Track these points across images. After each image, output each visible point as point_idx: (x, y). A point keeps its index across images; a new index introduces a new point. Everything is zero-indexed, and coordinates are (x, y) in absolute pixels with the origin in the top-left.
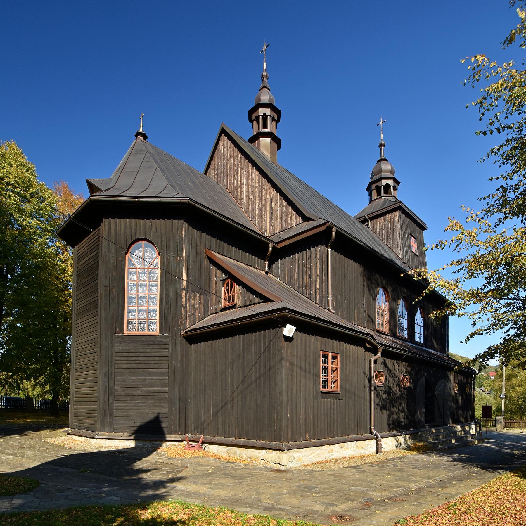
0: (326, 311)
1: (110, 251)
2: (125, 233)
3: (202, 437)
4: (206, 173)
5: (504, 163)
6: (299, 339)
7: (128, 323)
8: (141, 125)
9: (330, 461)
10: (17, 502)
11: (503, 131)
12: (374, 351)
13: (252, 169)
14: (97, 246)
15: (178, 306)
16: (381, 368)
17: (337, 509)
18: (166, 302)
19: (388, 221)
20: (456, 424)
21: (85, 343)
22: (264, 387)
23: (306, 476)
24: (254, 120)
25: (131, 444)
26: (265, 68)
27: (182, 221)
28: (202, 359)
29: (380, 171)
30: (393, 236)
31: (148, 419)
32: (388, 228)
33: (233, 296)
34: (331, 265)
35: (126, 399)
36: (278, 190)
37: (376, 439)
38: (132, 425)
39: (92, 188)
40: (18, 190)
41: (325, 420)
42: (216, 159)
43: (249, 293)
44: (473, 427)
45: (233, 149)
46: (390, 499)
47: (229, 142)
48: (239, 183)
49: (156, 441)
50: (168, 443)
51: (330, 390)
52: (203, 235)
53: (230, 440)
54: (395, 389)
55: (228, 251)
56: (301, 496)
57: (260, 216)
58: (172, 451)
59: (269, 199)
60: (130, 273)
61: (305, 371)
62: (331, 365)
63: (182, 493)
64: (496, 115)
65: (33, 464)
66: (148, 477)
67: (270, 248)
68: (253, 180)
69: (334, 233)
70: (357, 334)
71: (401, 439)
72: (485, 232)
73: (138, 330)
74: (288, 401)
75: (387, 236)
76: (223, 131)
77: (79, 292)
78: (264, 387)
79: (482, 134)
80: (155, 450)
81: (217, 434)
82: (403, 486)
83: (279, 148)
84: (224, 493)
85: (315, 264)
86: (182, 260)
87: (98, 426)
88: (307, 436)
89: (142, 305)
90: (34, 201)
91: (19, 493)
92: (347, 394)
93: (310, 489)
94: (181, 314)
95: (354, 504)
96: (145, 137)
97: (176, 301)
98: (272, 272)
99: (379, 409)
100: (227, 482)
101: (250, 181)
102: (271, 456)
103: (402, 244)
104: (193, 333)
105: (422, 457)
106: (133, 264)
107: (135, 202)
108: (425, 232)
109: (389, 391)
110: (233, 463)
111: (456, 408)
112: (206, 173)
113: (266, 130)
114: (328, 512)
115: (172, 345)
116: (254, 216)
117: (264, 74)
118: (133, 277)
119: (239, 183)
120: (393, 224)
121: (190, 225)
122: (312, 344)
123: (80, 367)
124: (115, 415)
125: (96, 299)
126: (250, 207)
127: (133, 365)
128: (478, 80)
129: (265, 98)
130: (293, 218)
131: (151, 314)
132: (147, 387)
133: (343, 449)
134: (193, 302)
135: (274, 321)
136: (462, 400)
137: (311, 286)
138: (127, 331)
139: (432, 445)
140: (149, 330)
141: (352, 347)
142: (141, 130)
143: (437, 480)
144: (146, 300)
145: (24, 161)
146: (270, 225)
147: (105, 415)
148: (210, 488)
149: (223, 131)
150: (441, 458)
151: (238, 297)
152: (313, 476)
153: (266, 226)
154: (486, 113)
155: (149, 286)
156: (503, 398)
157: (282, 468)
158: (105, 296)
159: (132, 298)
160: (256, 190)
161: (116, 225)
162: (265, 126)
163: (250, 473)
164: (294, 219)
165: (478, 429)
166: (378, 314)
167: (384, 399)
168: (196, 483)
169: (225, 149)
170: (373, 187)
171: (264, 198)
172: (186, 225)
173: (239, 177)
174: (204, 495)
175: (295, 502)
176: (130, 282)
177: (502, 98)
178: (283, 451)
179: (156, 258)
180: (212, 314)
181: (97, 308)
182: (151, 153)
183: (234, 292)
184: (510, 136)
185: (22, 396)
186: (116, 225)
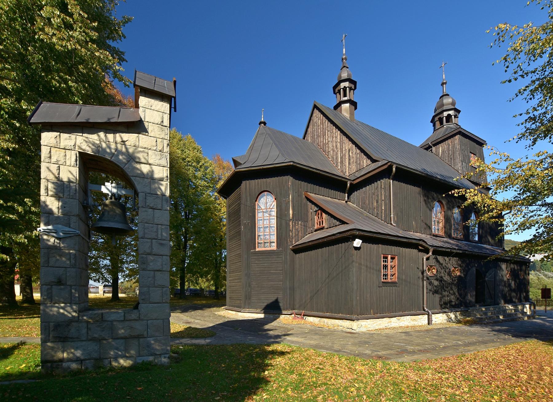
0: (389, 225)
1: (247, 201)
2: (255, 189)
3: (303, 312)
4: (304, 138)
5: (531, 99)
7: (258, 243)
10: (208, 341)
12: (426, 251)
14: (239, 198)
15: (288, 230)
16: (432, 262)
17: (379, 353)
18: (280, 229)
19: (449, 145)
20: (508, 303)
22: (342, 279)
23: (367, 336)
25: (262, 316)
29: (443, 105)
30: (454, 156)
31: (272, 301)
33: (322, 221)
36: (354, 142)
37: (428, 315)
38: (262, 304)
40: (193, 165)
42: (311, 126)
44: (528, 306)
46: (420, 351)
47: (319, 113)
49: (276, 314)
50: (283, 316)
52: (303, 183)
53: (321, 314)
54: (446, 278)
57: (342, 162)
58: (285, 320)
60: (258, 212)
61: (370, 268)
62: (389, 264)
63: (289, 341)
64: (519, 66)
65: (211, 325)
66: (271, 333)
68: (336, 137)
69: (394, 169)
71: (452, 315)
72: (505, 161)
74: (357, 288)
75: (448, 157)
76: (315, 107)
78: (342, 279)
79: (507, 82)
80: (275, 319)
81: (312, 310)
82: (434, 344)
83: (356, 108)
84: (312, 342)
85: (381, 193)
87: (242, 305)
90: (202, 170)
92: (404, 283)
93: (366, 343)
95: (392, 352)
96: (265, 123)
97: (286, 228)
99: (431, 293)
100: (316, 337)
101: (334, 139)
104: (297, 247)
106: (260, 207)
107: (260, 169)
108: (485, 148)
109: (441, 280)
111: (509, 291)
112: (304, 138)
113: (346, 98)
114: (373, 355)
116: (337, 163)
118: (260, 215)
126: (335, 157)
128: (503, 41)
129: (344, 75)
130: (365, 161)
131: (271, 236)
136: (515, 284)
139: (478, 320)
141: (408, 250)
145: (196, 145)
146: (349, 167)
149: (315, 107)
150: (483, 330)
151: (325, 222)
152: (372, 337)
153: (346, 169)
154: (511, 65)
155: (270, 219)
157: (353, 331)
158: (245, 228)
159: (260, 228)
160: (339, 144)
161: (250, 184)
162: (345, 95)
163: (331, 333)
164: (366, 162)
165: (532, 308)
166: (434, 221)
167: (436, 286)
168: (298, 337)
170: (436, 119)
172: (291, 178)
174: (301, 343)
175: (354, 348)
178: (353, 321)
182: (269, 135)
184: (534, 78)
185: (198, 288)
186: (250, 184)
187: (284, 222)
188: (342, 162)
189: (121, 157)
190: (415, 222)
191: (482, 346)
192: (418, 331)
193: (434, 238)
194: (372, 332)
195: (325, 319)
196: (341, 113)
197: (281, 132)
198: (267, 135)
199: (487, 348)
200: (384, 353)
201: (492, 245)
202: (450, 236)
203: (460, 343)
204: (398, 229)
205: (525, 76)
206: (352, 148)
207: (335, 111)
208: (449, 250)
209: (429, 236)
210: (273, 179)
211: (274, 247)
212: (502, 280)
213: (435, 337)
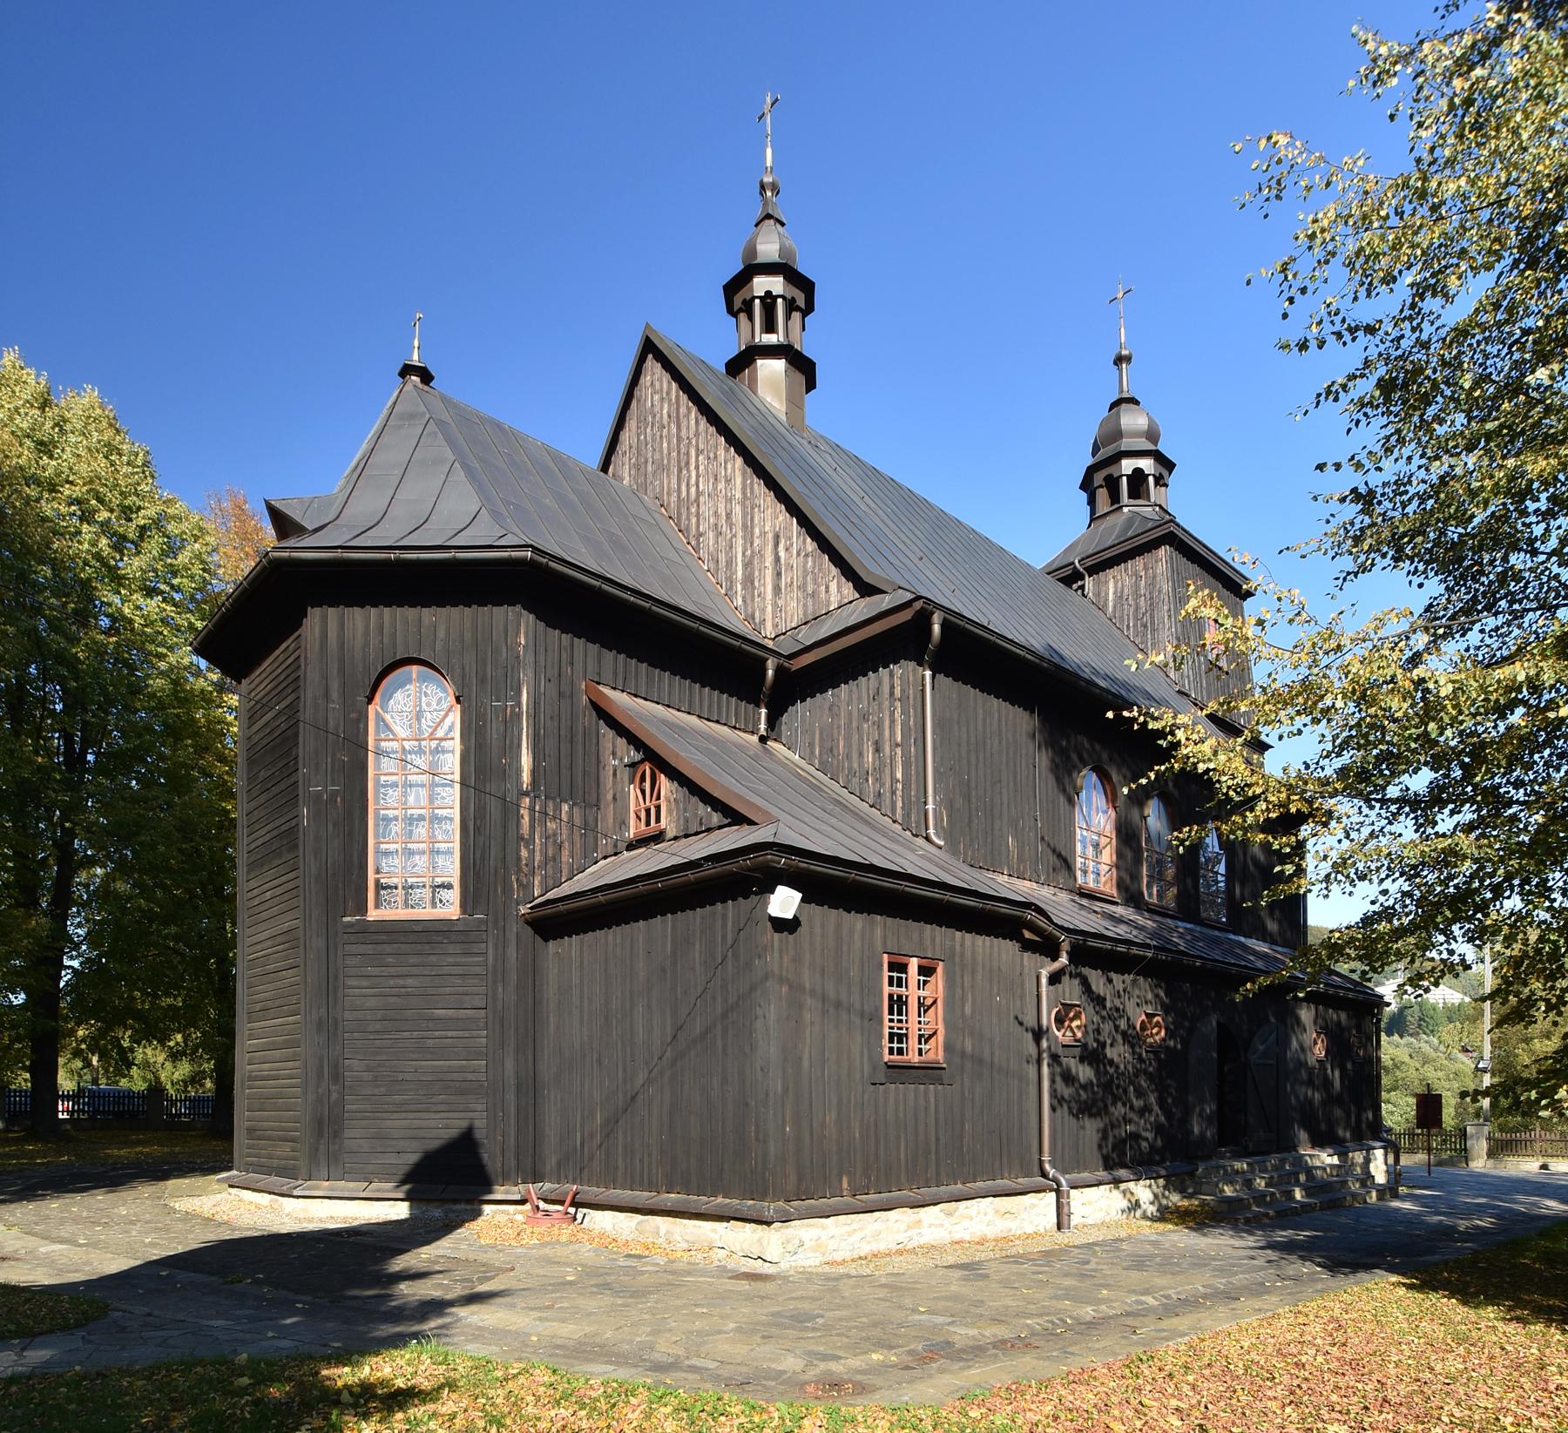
0: (920, 841)
1: (327, 695)
2: (366, 645)
4: (605, 468)
6: (818, 923)
8: (416, 344)
9: (913, 1251)
10: (38, 1355)
11: (1354, 340)
12: (1048, 948)
13: (727, 451)
14: (292, 682)
17: (835, 1367)
18: (477, 830)
21: (269, 943)
24: (740, 310)
26: (769, 164)
27: (518, 608)
28: (575, 980)
29: (1118, 434)
30: (1152, 617)
32: (1137, 596)
33: (658, 808)
34: (933, 715)
35: (376, 1091)
36: (793, 509)
37: (1058, 1192)
38: (392, 1159)
39: (283, 524)
41: (898, 1138)
43: (695, 799)
45: (677, 397)
46: (1000, 1344)
47: (666, 377)
48: (693, 490)
49: (455, 1201)
51: (913, 1057)
52: (580, 643)
54: (1117, 1053)
55: (649, 684)
56: (764, 1337)
57: (749, 581)
58: (502, 1227)
59: (770, 536)
62: (913, 993)
63: (479, 1334)
65: (115, 1265)
67: (770, 672)
68: (728, 481)
69: (936, 628)
70: (990, 905)
71: (1143, 1191)
72: (1291, 621)
73: (406, 905)
74: (786, 1090)
76: (649, 348)
77: (254, 804)
81: (610, 1181)
83: (811, 385)
85: (892, 714)
86: (519, 715)
88: (845, 1185)
89: (415, 837)
91: (51, 1331)
92: (968, 1065)
94: (519, 859)
96: (426, 376)
98: (780, 735)
100: (591, 1304)
101: (721, 485)
102: (732, 1241)
103: (1178, 639)
104: (549, 910)
105: (1180, 1238)
106: (387, 727)
107: (387, 562)
110: (640, 1257)
111: (1323, 1103)
112: (605, 468)
113: (771, 339)
115: (496, 945)
116: (731, 581)
117: (768, 179)
119: (693, 490)
120: (1152, 584)
121: (539, 617)
122: (857, 936)
123: (258, 1007)
124: (347, 1133)
125: (294, 823)
126: (722, 558)
127: (393, 999)
129: (769, 250)
130: (833, 587)
131: (440, 860)
132: (429, 1056)
133: (953, 1220)
134: (551, 825)
135: (744, 877)
137: (864, 780)
138: (377, 906)
139: (1224, 1207)
140: (434, 905)
142: (416, 357)
143: (1168, 1297)
144: (426, 824)
146: (775, 605)
147: (320, 1135)
148: (540, 1319)
149: (649, 348)
151: (669, 811)
152: (835, 1290)
153: (763, 610)
155: (433, 785)
156: (1484, 1071)
157: (767, 1269)
159: (387, 820)
160: (737, 510)
161: (342, 626)
162: (770, 327)
164: (837, 590)
169: (656, 397)
170: (1099, 478)
171: (757, 531)
172: (527, 619)
173: (694, 474)
176: (383, 778)
177: (1339, 259)
178: (768, 1224)
179: (450, 710)
180: (605, 858)
181: (296, 847)
182: (441, 424)
183: (658, 798)
186: (342, 626)
187: (493, 806)
188: (749, 581)
189: (1343, 968)
190: (1015, 837)
191: (1222, 1310)
192: (1017, 1259)
193: (1085, 902)
194: (841, 1270)
195: (658, 1220)
196: (754, 390)
197: (499, 426)
198: (432, 427)
199: (1236, 1317)
200: (856, 1362)
201: (1273, 942)
202: (1133, 898)
203: (1150, 1300)
204: (953, 861)
205: (1347, 337)
206: (788, 528)
207: (730, 381)
208: (1108, 946)
209: (1064, 896)
210: (443, 612)
211: (450, 907)
212: (1302, 1064)
213: (1069, 1282)
